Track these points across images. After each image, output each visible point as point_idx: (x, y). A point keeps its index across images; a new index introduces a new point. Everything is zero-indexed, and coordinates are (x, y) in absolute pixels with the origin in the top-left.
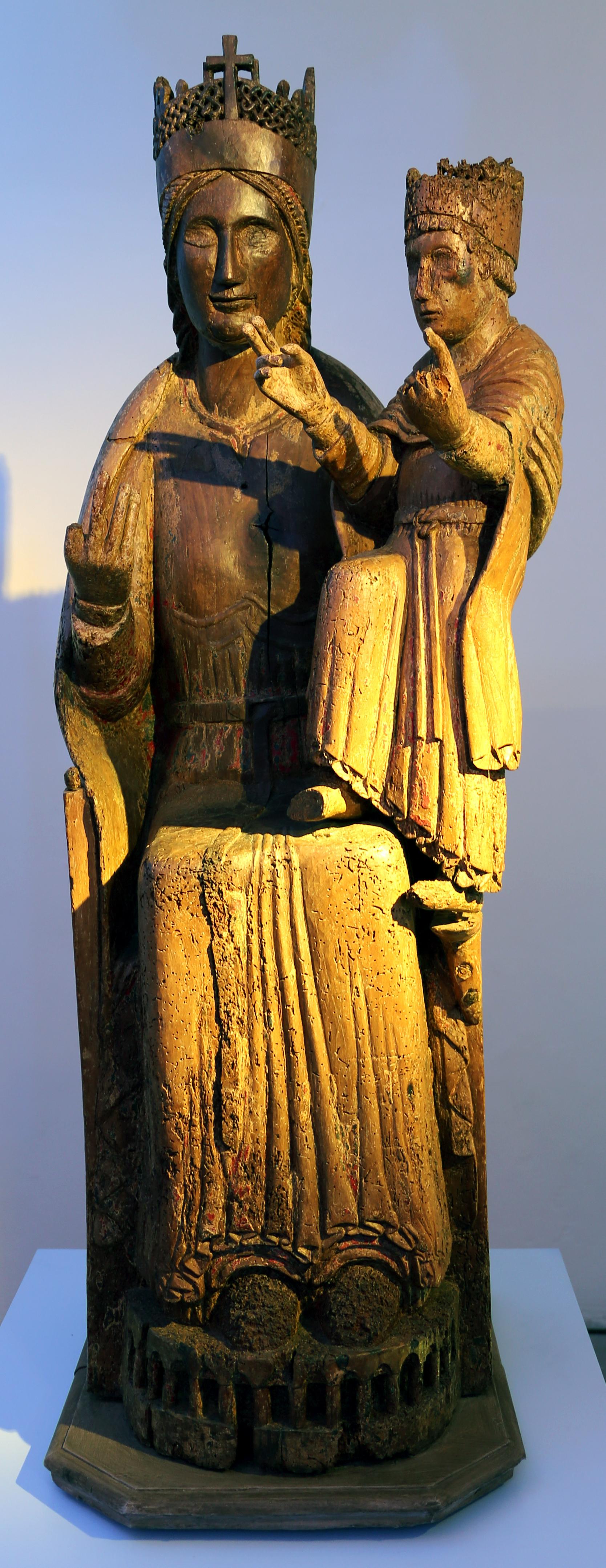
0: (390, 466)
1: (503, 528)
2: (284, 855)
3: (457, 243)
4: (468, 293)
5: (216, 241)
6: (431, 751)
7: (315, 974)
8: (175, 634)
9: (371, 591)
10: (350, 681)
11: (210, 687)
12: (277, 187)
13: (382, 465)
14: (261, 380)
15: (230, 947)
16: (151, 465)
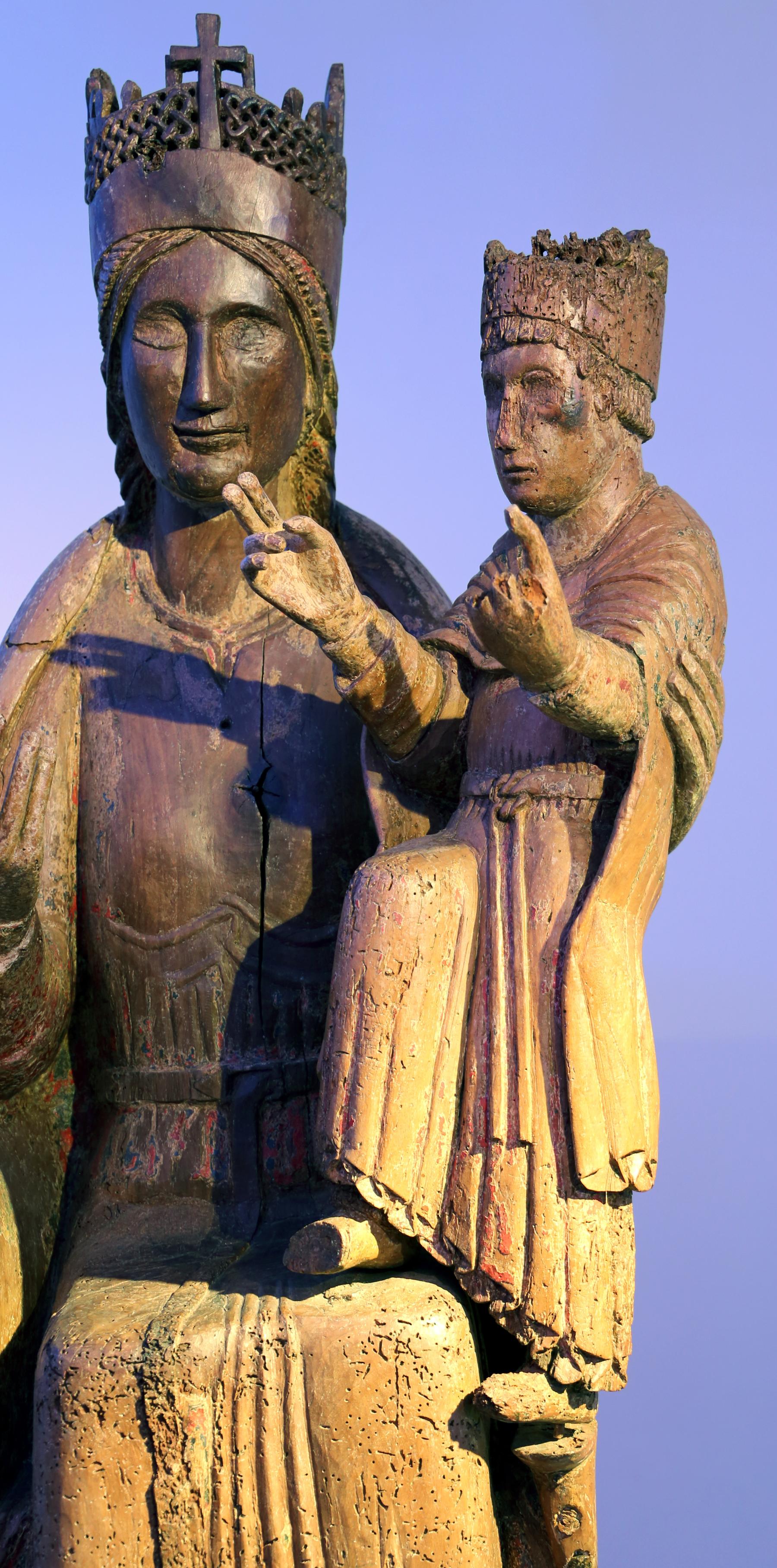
0: (456, 703)
1: (629, 809)
2: (276, 1332)
3: (562, 363)
4: (578, 440)
5: (184, 340)
6: (515, 1162)
7: (322, 1533)
8: (109, 957)
9: (422, 905)
10: (386, 1048)
11: (165, 1046)
12: (282, 258)
13: (443, 701)
14: (251, 572)
15: (184, 1489)
16: (77, 687)
